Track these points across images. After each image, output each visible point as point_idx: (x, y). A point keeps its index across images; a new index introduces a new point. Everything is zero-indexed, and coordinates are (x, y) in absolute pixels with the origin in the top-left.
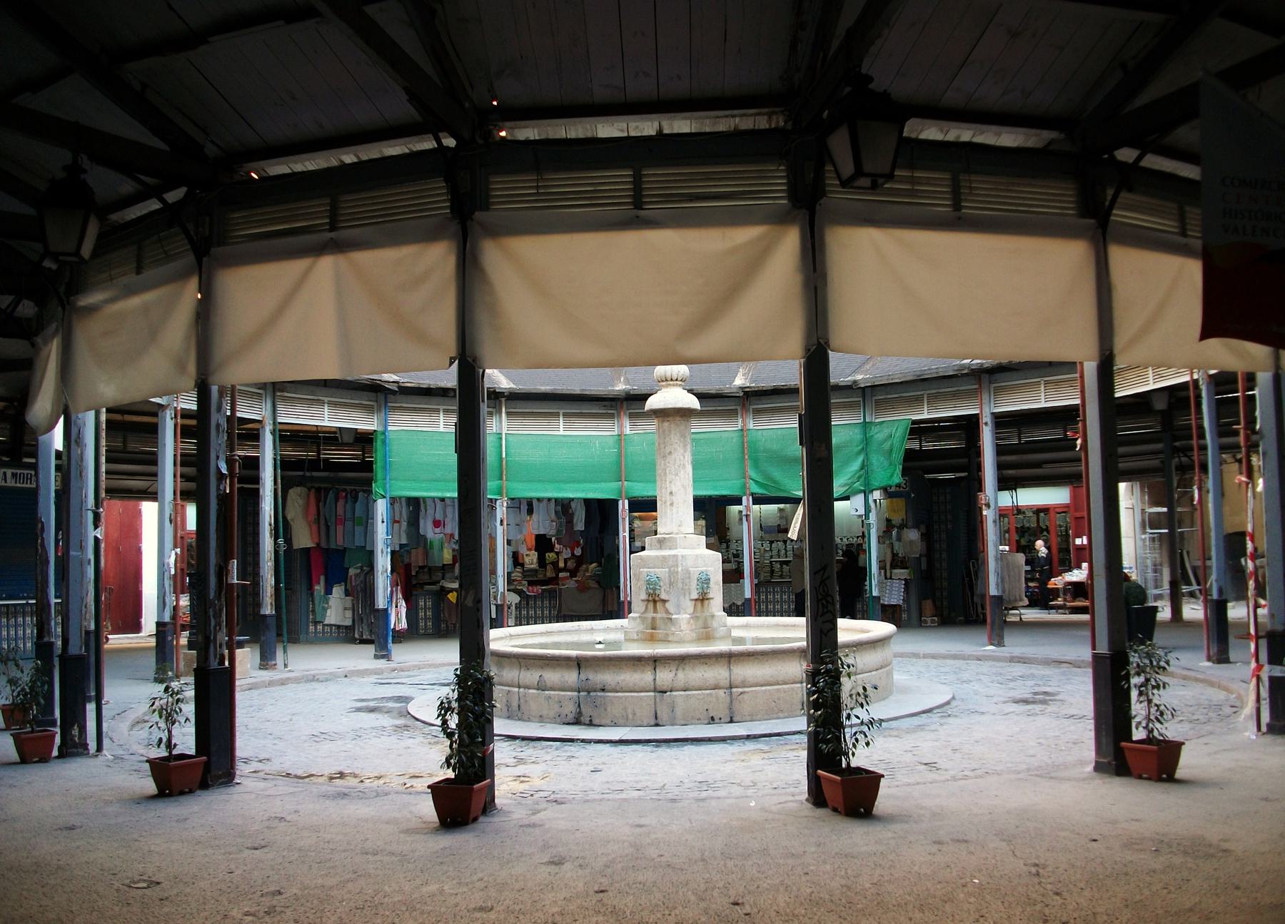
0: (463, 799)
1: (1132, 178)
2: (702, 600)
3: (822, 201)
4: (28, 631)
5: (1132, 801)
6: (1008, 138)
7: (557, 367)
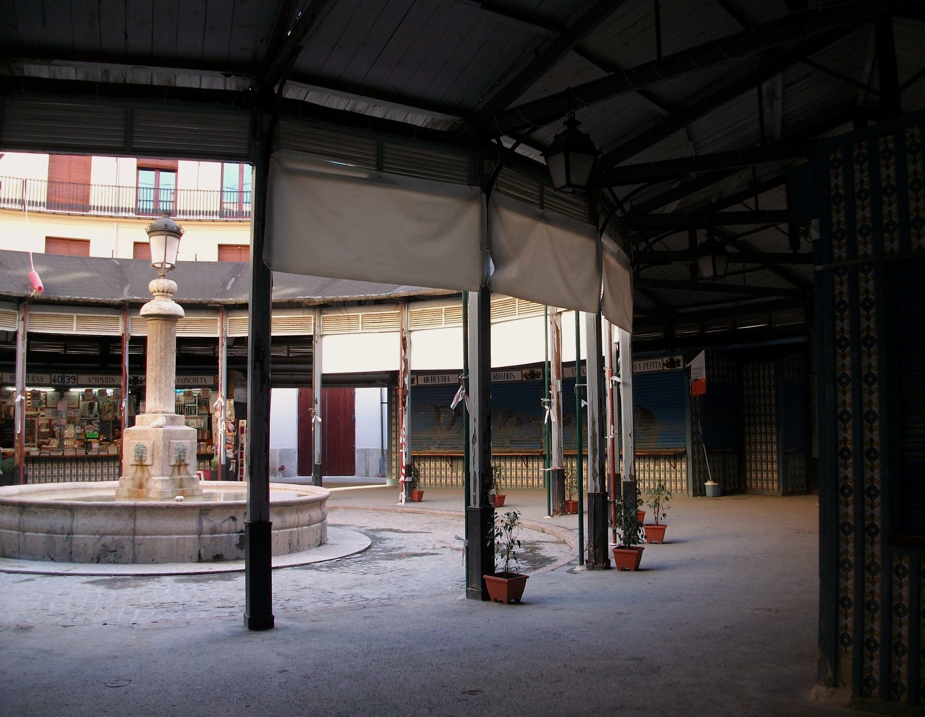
0: (260, 614)
1: (511, 158)
2: (179, 466)
3: (273, 155)
4: (427, 473)
5: (495, 618)
6: (419, 118)
7: (359, 280)
